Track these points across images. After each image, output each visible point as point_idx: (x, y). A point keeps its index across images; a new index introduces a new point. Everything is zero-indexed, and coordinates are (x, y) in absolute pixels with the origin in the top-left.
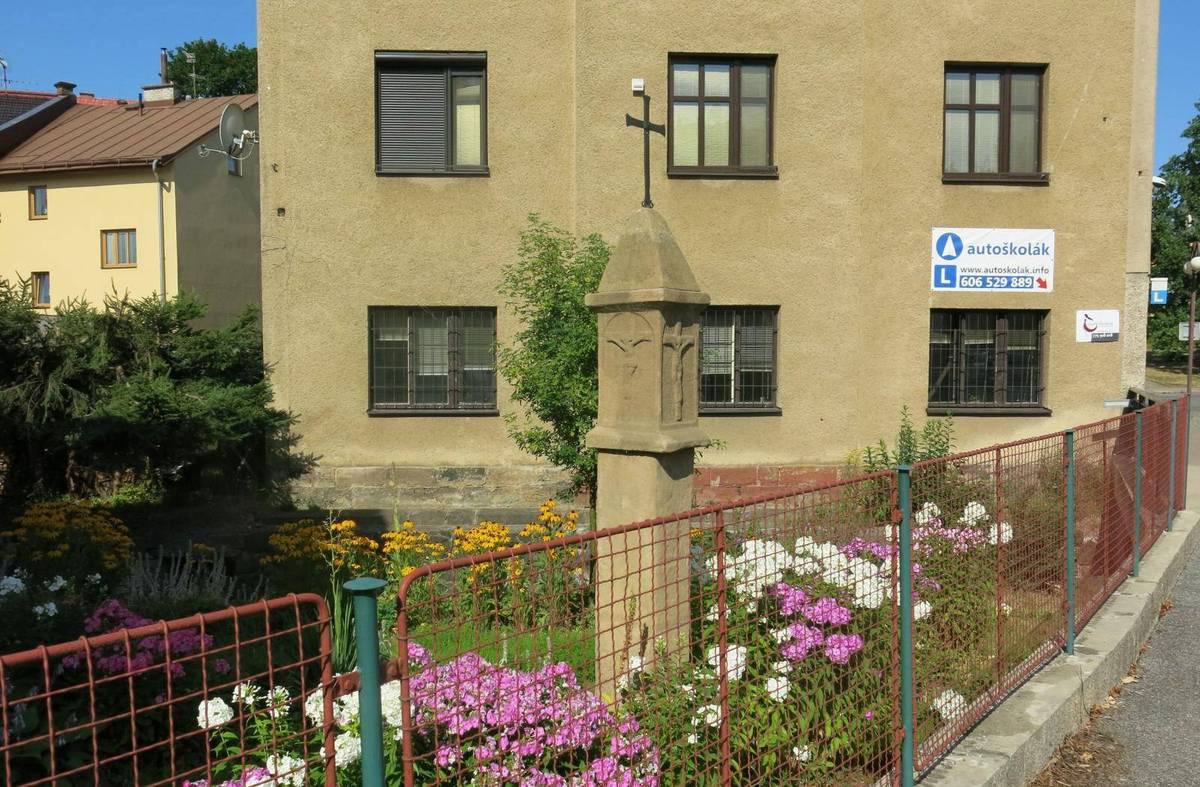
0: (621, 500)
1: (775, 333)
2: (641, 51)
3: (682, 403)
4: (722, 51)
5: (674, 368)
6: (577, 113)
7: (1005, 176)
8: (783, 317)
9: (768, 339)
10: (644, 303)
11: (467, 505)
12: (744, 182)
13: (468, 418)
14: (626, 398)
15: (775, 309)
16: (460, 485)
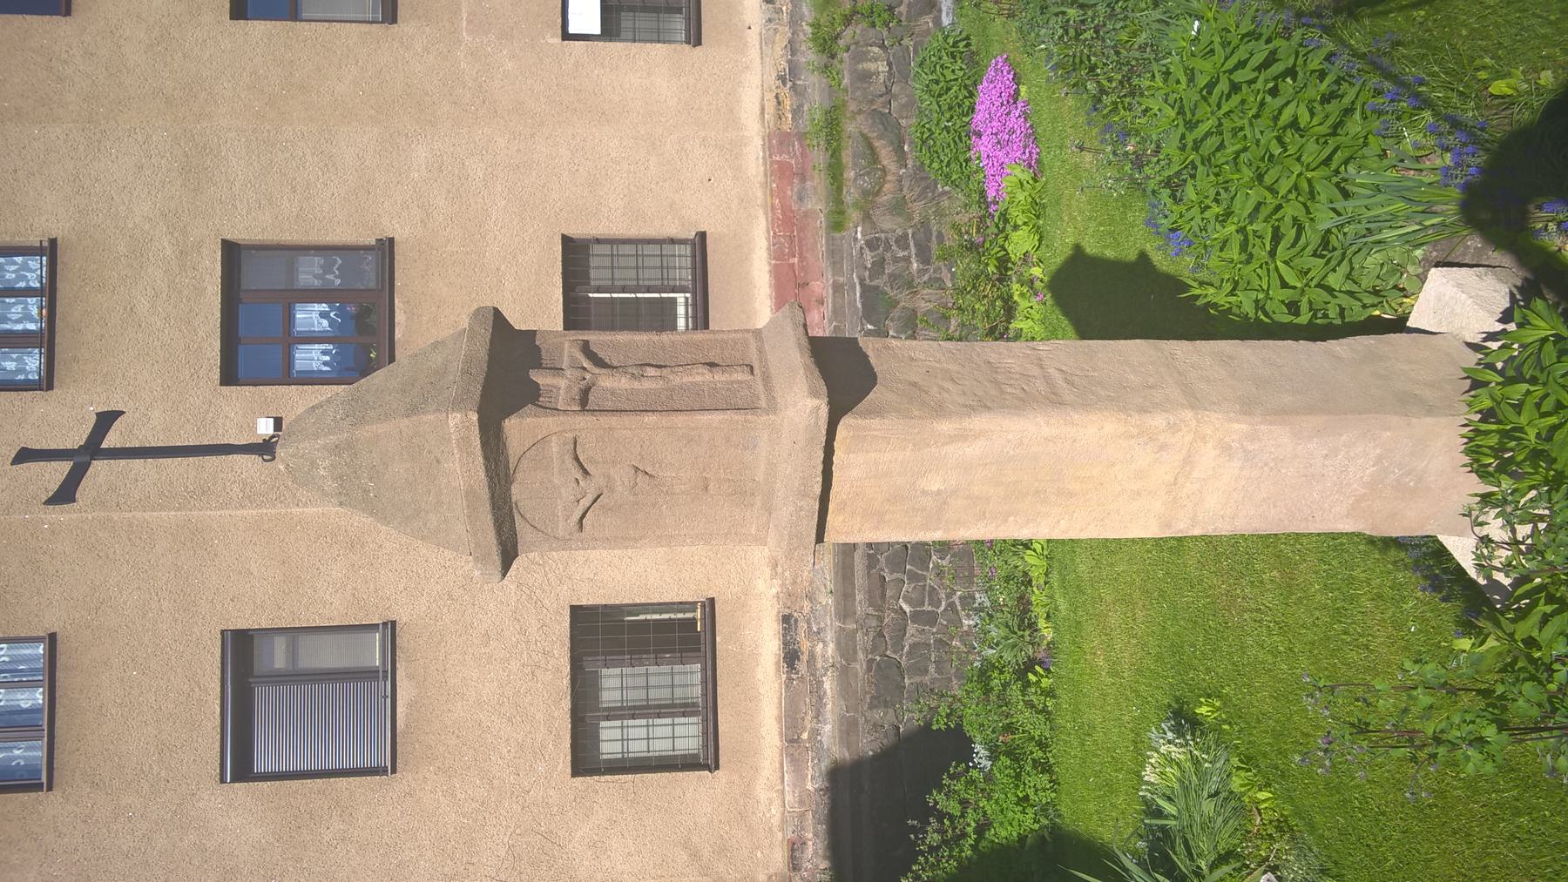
0: (924, 493)
1: (598, 241)
2: (220, 422)
3: (712, 365)
5: (636, 385)
6: (306, 505)
8: (577, 231)
10: (486, 458)
11: (829, 636)
12: (398, 283)
13: (718, 639)
15: (567, 241)
16: (805, 645)
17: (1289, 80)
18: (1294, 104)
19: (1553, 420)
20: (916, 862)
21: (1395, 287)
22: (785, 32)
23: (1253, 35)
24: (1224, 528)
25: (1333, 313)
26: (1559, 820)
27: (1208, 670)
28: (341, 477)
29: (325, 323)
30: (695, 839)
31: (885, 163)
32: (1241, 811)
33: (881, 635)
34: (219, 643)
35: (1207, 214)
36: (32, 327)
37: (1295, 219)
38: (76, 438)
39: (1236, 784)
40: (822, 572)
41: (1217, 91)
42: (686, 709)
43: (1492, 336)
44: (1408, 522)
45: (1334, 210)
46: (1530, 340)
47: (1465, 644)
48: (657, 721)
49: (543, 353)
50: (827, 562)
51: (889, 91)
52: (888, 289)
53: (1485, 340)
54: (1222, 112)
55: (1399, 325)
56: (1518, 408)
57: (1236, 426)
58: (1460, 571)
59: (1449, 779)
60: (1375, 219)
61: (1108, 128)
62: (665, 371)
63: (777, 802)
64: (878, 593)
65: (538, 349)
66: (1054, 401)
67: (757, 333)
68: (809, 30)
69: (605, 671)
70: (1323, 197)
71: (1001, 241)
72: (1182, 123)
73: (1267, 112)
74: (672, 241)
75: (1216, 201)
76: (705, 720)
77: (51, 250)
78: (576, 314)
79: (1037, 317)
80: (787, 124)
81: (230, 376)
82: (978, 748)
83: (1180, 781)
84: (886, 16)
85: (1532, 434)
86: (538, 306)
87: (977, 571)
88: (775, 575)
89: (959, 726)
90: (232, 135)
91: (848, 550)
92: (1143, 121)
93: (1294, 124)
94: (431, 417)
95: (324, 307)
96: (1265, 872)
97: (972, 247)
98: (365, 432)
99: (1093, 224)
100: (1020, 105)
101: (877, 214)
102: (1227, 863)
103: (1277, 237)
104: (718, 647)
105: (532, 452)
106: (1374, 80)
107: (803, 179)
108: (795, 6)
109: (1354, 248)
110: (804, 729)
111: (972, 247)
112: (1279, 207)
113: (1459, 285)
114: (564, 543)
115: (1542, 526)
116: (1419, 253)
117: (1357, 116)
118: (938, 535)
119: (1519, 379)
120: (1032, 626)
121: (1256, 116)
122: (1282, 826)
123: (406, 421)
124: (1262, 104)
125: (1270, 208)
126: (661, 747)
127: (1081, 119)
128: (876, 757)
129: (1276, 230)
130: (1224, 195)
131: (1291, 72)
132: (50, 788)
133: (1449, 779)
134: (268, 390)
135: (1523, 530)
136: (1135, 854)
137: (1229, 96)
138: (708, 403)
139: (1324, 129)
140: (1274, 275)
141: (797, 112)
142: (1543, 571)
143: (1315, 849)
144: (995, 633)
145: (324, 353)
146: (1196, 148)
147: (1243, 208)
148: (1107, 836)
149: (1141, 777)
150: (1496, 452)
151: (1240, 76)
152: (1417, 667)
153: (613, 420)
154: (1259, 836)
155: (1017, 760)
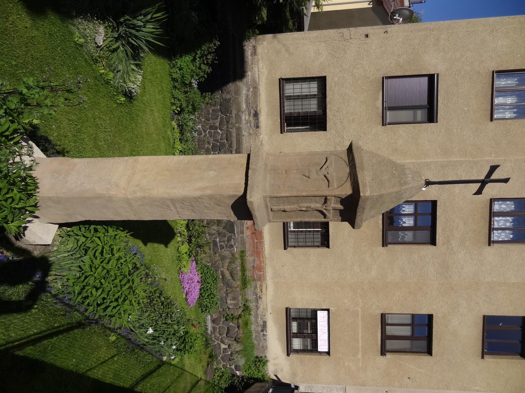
0: (215, 171)
1: (318, 246)
3: (284, 211)
4: (437, 223)
5: (309, 205)
6: (411, 163)
7: (385, 337)
8: (325, 249)
9: (316, 244)
10: (357, 181)
11: (244, 122)
12: (381, 233)
14: (286, 171)
15: (328, 246)
16: (252, 119)
17: (99, 303)
18: (97, 295)
19: (8, 196)
20: (215, 49)
21: (63, 237)
22: (259, 312)
23: (111, 316)
24: (117, 159)
25: (83, 229)
26: (2, 63)
27: (121, 112)
28: (404, 174)
29: (404, 220)
30: (287, 56)
31: (228, 272)
32: (109, 66)
33: (227, 122)
34: (438, 119)
35: (125, 259)
36: (496, 218)
37: (96, 259)
38: (489, 186)
39: (111, 75)
40: (247, 143)
41: (122, 299)
42: (290, 98)
43: (29, 222)
44: (57, 161)
45: (84, 262)
46: (16, 222)
47: (35, 122)
48: (299, 94)
49: (339, 214)
50: (245, 144)
51: (227, 294)
52: (226, 232)
53: (32, 220)
54: (120, 292)
55: (61, 225)
56: (20, 199)
57: (114, 193)
58: (38, 146)
59: (40, 77)
60: (70, 260)
61: (158, 285)
62: (299, 209)
63: (260, 68)
64: (228, 136)
65: (340, 216)
66: (173, 201)
67: (270, 221)
68: (252, 313)
69: (316, 110)
70: (87, 266)
71: (191, 248)
72: (134, 288)
73: (106, 293)
74: (294, 247)
75: (122, 264)
76: (283, 94)
77: (490, 242)
78: (325, 226)
79: (179, 225)
80: (258, 283)
81: (434, 203)
82: (196, 86)
83: (130, 76)
84: (228, 318)
85: (15, 191)
86: (339, 229)
87: (197, 143)
88: (261, 141)
89: (202, 94)
90: (433, 278)
91: (238, 151)
92: (146, 288)
93: (97, 289)
94: (375, 194)
95: (404, 225)
96: (101, 46)
97: (200, 246)
98: (396, 189)
99: (162, 254)
100: (185, 292)
101: (230, 256)
102: (114, 49)
103: (102, 253)
104: (279, 118)
106: (72, 303)
107: (253, 267)
108: (257, 320)
109: (76, 250)
110: (252, 92)
111: (200, 246)
112: (101, 262)
113: (41, 239)
115: (11, 161)
116: (55, 248)
117: (77, 292)
118: (211, 156)
119: (20, 209)
120: (179, 126)
121: (109, 291)
122: (96, 61)
124: (108, 295)
125: (105, 262)
126: (298, 86)
127: (166, 288)
128: (229, 83)
129: (102, 255)
130: (119, 265)
131: (98, 305)
132: (493, 71)
133: (40, 77)
134: (422, 199)
135: (17, 159)
136: (144, 51)
137: (119, 297)
139: (87, 288)
140: (102, 241)
141: (256, 287)
142: (10, 147)
143: (85, 53)
144: (191, 123)
145: (404, 211)
146: (129, 280)
147: (113, 262)
148: (153, 57)
149: (143, 77)
150: (27, 186)
151: (115, 304)
152: (51, 112)
153: (316, 193)
154: (103, 58)
155: (183, 82)
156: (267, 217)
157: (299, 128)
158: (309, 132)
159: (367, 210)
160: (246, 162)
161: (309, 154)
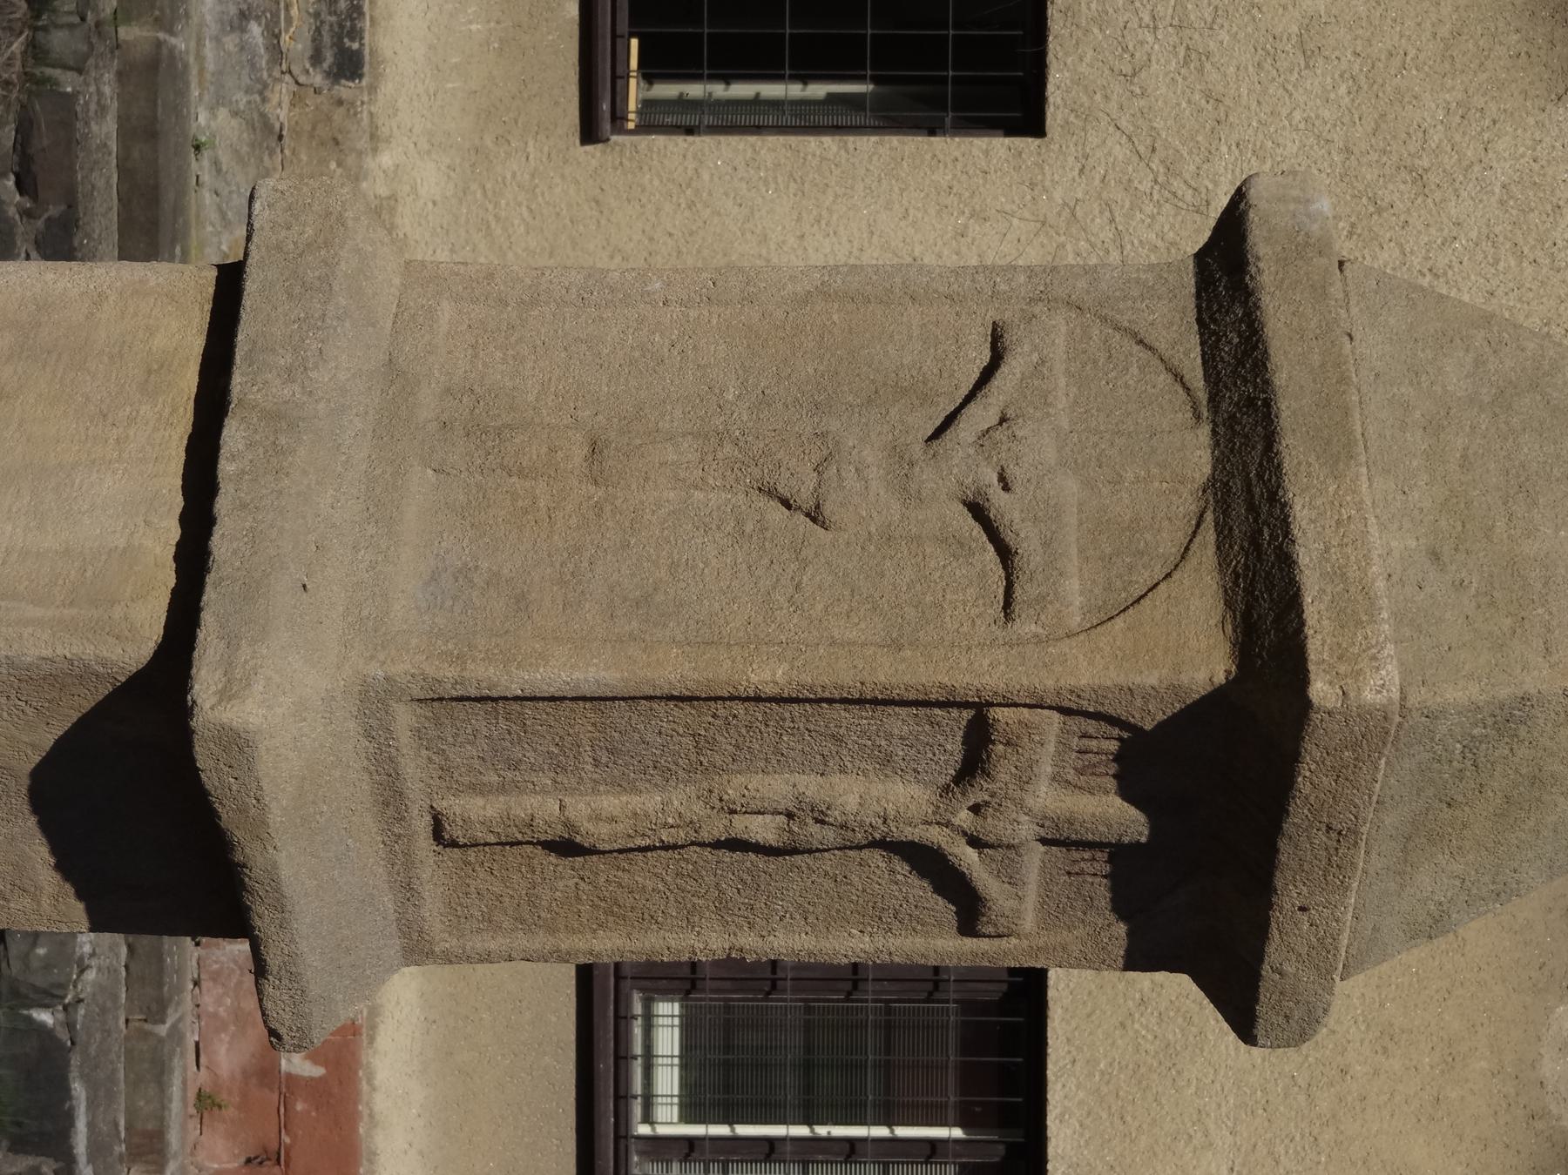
3: (566, 847)
5: (811, 786)
10: (1286, 561)
49: (1101, 892)
62: (716, 828)
64: (43, 140)
65: (1122, 907)
67: (417, 950)
86: (1119, 1035)
91: (148, 230)
94: (1455, 694)
105: (1143, 579)
114: (1047, 289)
123: (1530, 684)
138: (583, 722)
153: (887, 673)
156: (388, 902)
157: (772, 90)
158: (866, 144)
159: (1372, 859)
160: (196, 344)
161: (823, 291)
